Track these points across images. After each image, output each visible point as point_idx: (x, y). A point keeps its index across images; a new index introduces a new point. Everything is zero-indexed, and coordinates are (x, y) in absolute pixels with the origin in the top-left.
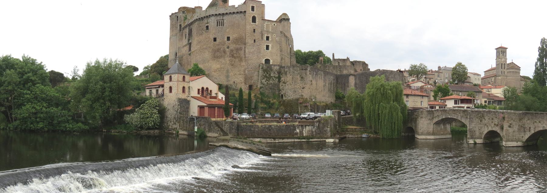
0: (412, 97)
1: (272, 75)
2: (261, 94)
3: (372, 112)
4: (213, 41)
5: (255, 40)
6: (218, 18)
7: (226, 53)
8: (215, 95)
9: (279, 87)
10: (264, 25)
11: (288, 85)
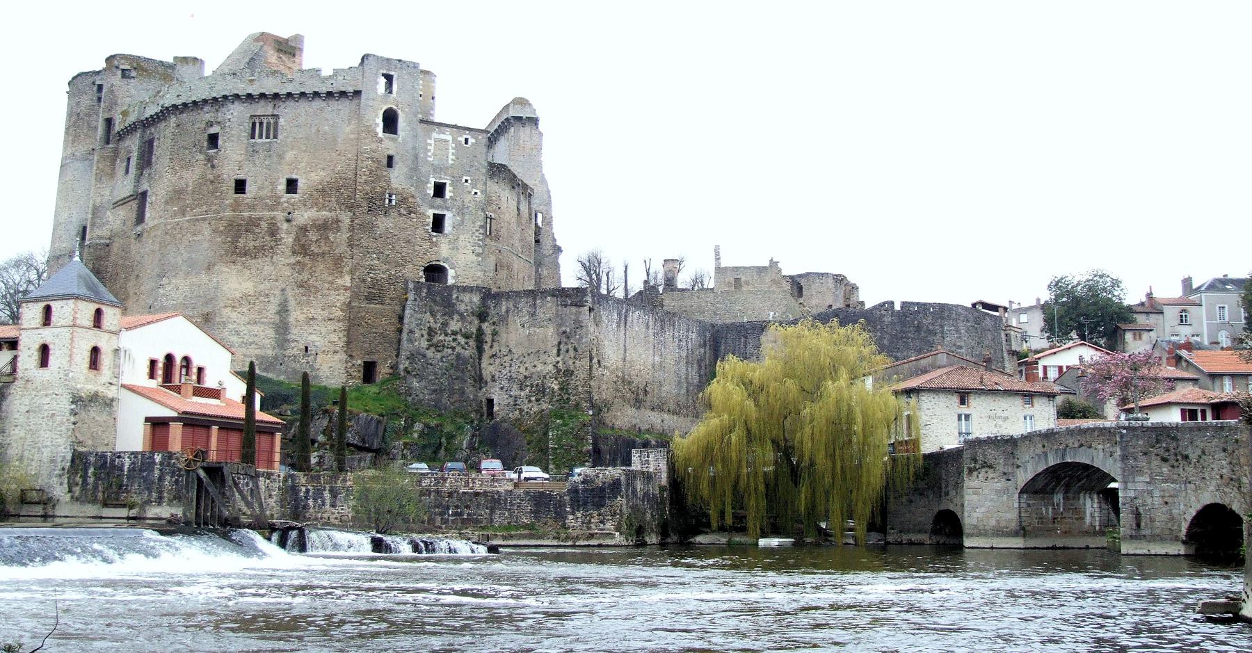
0: (983, 398)
6: (263, 109)
10: (429, 141)
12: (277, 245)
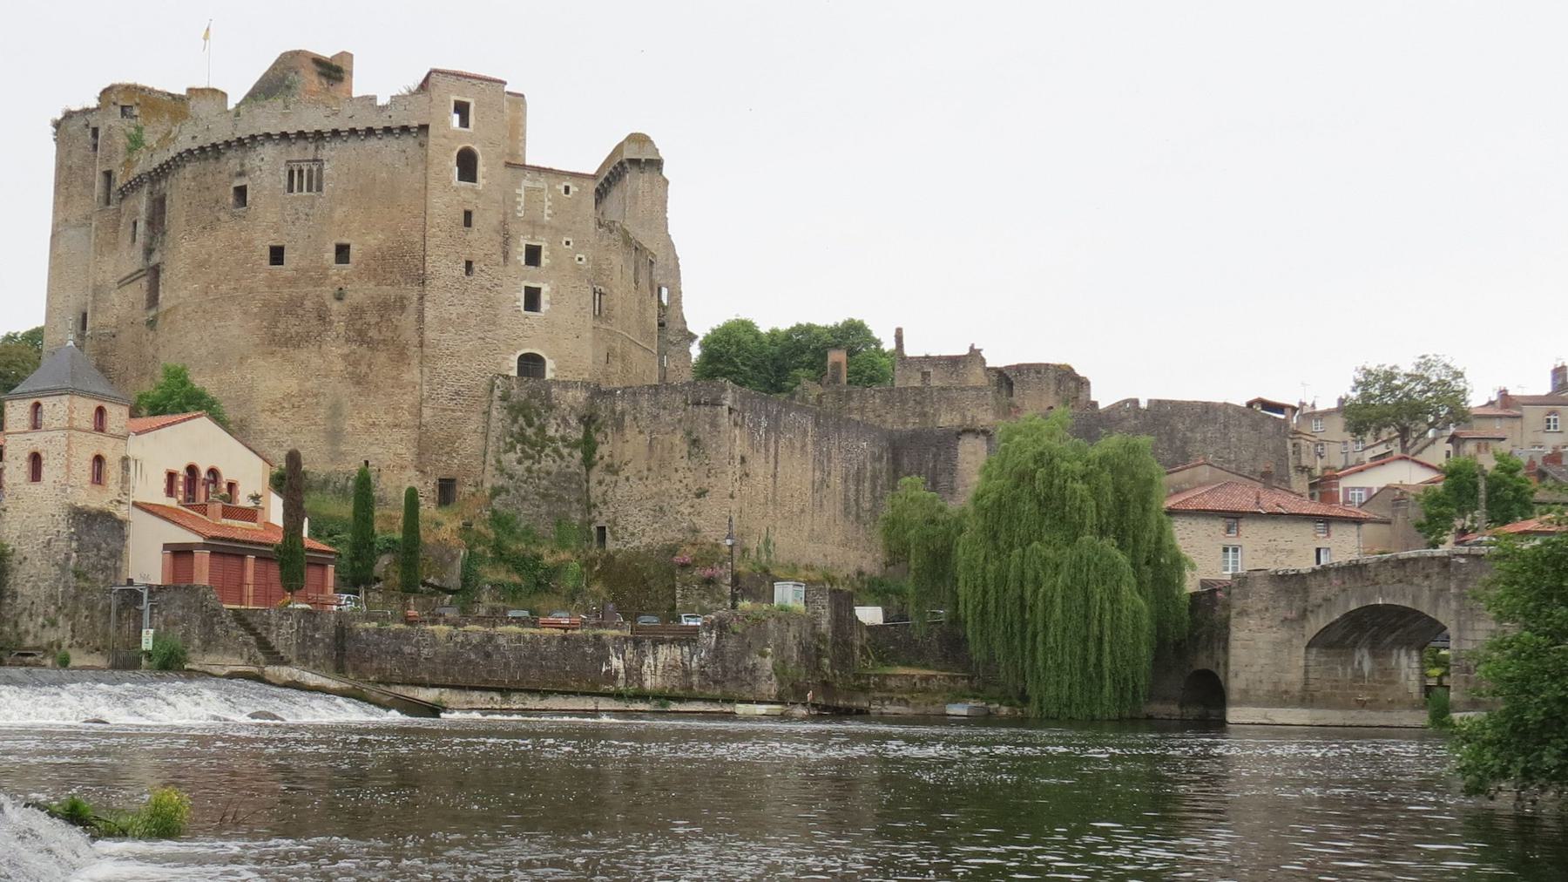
1: (551, 432)
2: (498, 520)
3: (992, 591)
4: (266, 262)
5: (469, 265)
6: (296, 152)
7: (331, 323)
8: (251, 504)
9: (588, 490)
11: (627, 479)
12: (325, 330)
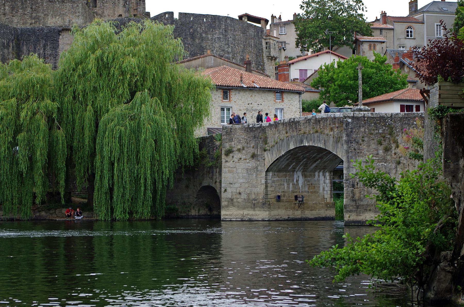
0: (242, 93)
